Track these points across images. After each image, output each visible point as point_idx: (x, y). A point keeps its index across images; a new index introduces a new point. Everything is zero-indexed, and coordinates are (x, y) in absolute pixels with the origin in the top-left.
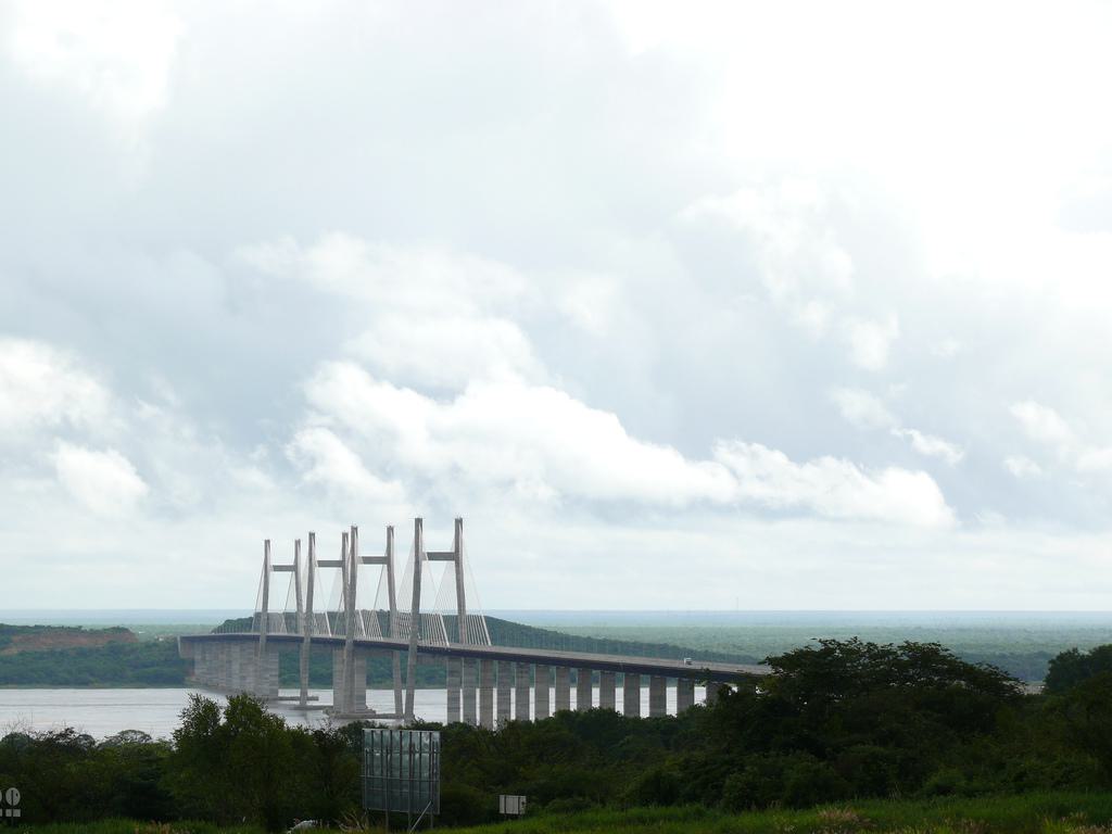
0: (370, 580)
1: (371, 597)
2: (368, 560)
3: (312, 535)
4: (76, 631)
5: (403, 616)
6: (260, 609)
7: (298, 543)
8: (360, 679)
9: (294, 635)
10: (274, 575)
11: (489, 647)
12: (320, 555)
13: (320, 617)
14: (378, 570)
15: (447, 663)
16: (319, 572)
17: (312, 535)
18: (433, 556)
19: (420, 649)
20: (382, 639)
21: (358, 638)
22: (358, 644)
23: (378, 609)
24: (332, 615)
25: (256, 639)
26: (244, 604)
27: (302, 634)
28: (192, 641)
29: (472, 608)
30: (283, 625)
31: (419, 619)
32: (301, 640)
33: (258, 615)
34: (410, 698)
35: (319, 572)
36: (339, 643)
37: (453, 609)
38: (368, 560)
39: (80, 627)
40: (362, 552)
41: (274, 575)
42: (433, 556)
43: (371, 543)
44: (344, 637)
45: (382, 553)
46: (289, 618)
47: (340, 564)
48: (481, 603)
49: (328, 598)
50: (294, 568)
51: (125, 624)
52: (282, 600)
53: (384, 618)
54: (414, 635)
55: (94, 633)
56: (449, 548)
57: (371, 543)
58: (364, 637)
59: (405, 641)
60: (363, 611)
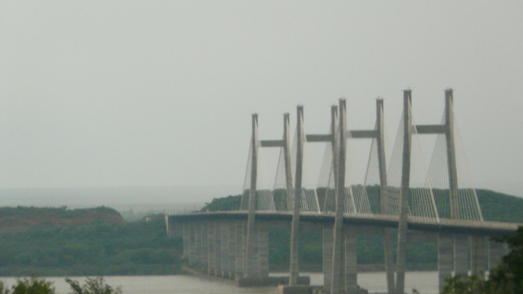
0: (359, 152)
1: (360, 170)
2: (357, 134)
3: (300, 109)
4: (60, 213)
5: (392, 190)
6: (248, 187)
7: (286, 117)
8: (350, 259)
9: (283, 212)
10: (417, 139)
11: (481, 223)
12: (308, 130)
13: (310, 193)
14: (367, 144)
15: (440, 242)
16: (308, 147)
17: (300, 109)
18: (423, 129)
19: (412, 226)
20: (370, 216)
21: (347, 214)
22: (349, 222)
23: (367, 184)
24: (321, 192)
25: (244, 217)
26: (235, 185)
27: (291, 213)
28: (180, 220)
29: (463, 184)
30: (273, 204)
31: (410, 195)
32: (289, 218)
33: (247, 193)
34: (401, 278)
35: (308, 147)
36: (328, 221)
37: (444, 184)
38: (357, 134)
39: (65, 207)
40: (417, 120)
41: (262, 151)
42: (423, 129)
43: (360, 118)
44: (334, 214)
45: (371, 126)
46: (279, 195)
47: (329, 138)
48: (470, 180)
49: (316, 174)
50: (283, 143)
51: (108, 203)
52: (270, 179)
53: (375, 194)
54: (404, 212)
55: (81, 214)
56: (438, 120)
57: (360, 118)
58: (354, 213)
59: (395, 217)
60: (353, 187)
